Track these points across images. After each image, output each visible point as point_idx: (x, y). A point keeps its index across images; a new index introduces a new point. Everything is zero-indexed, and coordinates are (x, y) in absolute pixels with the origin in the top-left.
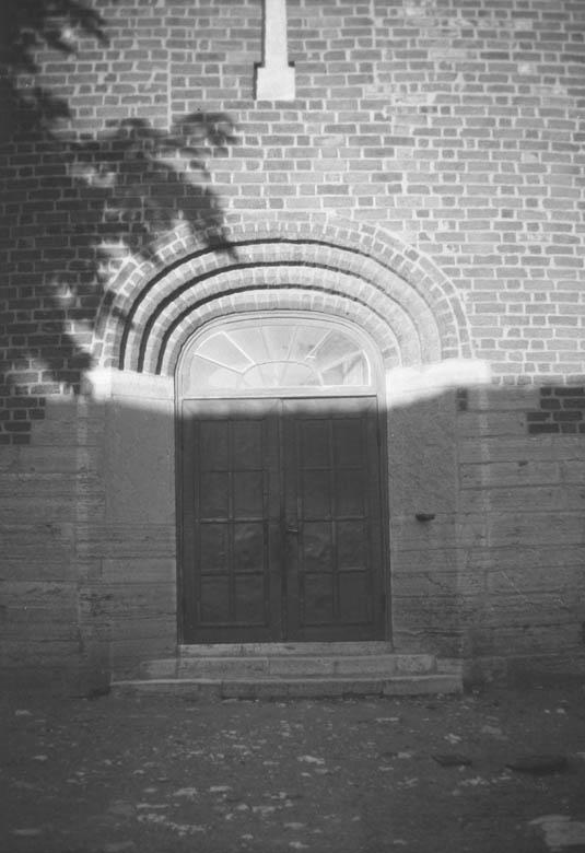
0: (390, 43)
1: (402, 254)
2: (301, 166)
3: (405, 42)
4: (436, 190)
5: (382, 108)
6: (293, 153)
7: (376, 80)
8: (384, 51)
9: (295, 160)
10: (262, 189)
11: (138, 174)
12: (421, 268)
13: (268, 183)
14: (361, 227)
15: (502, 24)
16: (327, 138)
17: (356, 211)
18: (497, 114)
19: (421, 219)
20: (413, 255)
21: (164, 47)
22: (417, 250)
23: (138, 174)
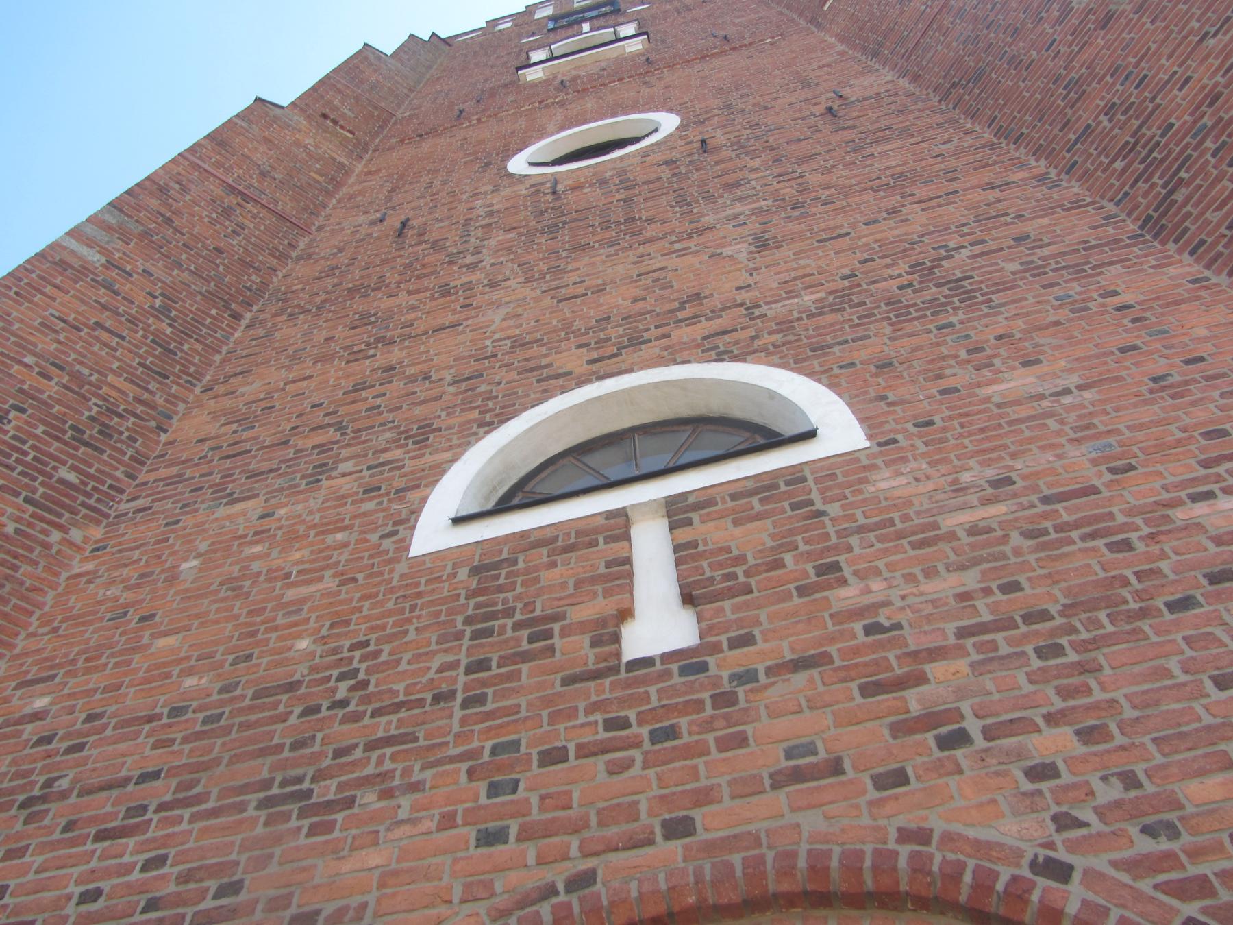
0: (861, 529)
1: (1026, 872)
2: (725, 744)
3: (19, 474)
4: (1051, 719)
5: (877, 615)
6: (708, 726)
7: (852, 579)
8: (854, 541)
9: (710, 738)
10: (643, 807)
11: (808, 548)
12: (1090, 896)
13: (656, 791)
14: (893, 835)
15: (1060, 457)
16: (773, 684)
17: (871, 803)
18: (785, 492)
19: (1044, 786)
20: (1061, 872)
21: (460, 626)
22: (1062, 855)
23: (808, 548)
